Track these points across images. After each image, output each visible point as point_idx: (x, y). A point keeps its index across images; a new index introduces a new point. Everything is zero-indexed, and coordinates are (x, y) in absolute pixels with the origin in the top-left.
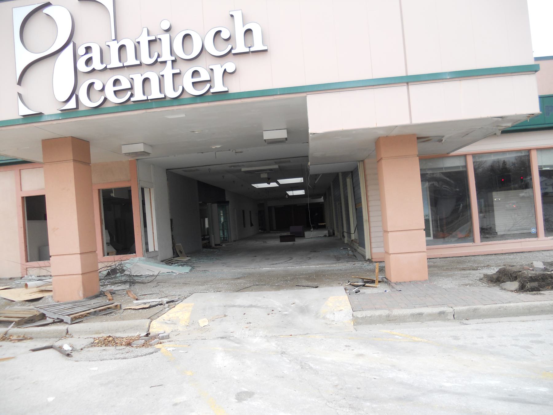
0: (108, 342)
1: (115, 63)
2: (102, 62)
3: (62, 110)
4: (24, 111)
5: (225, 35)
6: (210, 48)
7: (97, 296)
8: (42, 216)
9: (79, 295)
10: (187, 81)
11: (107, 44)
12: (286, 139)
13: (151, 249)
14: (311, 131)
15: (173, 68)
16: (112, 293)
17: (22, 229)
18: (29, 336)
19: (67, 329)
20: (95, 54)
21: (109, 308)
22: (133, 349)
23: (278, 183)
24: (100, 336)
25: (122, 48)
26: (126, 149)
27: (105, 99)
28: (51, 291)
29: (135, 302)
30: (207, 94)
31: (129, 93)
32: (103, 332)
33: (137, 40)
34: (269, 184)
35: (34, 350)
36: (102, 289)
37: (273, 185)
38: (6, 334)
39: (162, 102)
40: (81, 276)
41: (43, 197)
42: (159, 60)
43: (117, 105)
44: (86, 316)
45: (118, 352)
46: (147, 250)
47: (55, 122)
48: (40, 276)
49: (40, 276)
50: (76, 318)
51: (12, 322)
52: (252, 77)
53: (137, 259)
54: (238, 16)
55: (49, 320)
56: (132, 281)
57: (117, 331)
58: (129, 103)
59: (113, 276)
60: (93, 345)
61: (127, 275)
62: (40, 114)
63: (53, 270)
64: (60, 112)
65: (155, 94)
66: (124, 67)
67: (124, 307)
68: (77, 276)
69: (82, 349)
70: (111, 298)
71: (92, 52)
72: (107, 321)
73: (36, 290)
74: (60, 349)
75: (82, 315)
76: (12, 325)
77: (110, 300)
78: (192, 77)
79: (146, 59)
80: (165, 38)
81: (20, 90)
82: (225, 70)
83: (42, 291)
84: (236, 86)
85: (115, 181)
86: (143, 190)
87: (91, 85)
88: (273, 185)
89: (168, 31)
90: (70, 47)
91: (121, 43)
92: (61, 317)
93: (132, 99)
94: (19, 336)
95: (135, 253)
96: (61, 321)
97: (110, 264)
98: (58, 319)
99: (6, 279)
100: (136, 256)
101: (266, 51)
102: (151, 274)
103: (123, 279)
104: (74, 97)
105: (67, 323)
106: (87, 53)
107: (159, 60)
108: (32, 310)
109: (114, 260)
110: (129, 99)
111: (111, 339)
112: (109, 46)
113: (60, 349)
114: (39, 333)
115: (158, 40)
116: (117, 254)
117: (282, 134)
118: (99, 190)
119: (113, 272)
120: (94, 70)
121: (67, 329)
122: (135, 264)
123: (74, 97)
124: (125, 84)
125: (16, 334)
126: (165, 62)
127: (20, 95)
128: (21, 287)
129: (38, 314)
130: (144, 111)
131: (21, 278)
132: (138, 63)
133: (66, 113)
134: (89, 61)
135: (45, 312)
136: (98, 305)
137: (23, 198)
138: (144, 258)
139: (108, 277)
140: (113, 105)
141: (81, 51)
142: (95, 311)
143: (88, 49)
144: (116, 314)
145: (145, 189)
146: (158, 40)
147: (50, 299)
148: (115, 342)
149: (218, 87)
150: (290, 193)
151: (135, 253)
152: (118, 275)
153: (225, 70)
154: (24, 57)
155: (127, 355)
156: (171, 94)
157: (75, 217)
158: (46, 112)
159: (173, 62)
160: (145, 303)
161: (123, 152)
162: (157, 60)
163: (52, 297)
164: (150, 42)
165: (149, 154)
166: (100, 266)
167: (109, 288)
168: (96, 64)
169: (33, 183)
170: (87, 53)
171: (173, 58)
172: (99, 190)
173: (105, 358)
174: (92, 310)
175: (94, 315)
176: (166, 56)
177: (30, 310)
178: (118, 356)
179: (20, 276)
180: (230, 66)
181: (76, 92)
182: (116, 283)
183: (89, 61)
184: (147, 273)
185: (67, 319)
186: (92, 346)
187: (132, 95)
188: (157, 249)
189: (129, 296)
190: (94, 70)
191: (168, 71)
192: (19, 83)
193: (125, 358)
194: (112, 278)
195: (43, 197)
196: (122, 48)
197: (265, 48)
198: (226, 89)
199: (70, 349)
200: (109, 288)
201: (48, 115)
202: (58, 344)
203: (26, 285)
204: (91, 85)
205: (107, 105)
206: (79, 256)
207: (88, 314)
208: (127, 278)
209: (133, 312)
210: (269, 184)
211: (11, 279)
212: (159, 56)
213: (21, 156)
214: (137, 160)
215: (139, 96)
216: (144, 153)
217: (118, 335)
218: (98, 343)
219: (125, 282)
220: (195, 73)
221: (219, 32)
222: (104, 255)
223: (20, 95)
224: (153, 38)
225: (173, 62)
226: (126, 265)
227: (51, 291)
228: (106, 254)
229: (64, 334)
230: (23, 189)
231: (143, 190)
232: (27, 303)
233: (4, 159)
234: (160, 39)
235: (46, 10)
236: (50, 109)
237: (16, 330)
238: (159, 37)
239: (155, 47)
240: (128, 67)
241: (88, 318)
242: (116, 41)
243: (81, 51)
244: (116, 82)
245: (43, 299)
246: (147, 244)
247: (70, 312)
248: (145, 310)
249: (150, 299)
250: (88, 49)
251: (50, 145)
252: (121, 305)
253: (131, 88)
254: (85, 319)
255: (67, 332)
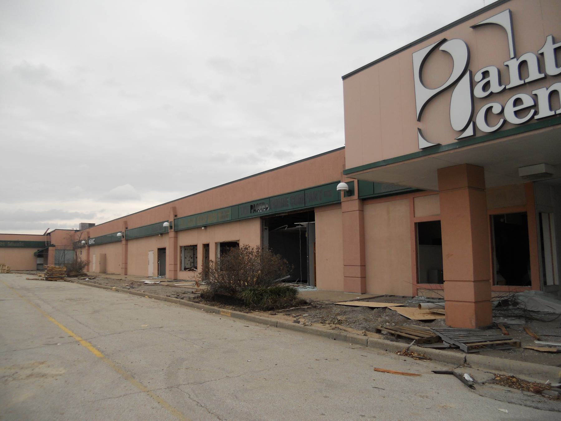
0: (511, 382)
1: (515, 81)
2: (500, 84)
4: (424, 144)
7: (489, 328)
8: (438, 242)
9: (471, 323)
10: (509, 111)
11: (506, 64)
13: (550, 282)
16: (507, 326)
18: (428, 357)
19: (465, 358)
20: (493, 78)
21: (506, 344)
22: (543, 399)
24: (501, 373)
25: (523, 65)
26: (523, 172)
27: (505, 122)
28: (444, 315)
29: (537, 342)
31: (532, 111)
32: (504, 370)
33: (540, 52)
35: (436, 372)
36: (495, 320)
38: (408, 349)
40: (473, 304)
43: (517, 126)
44: (482, 347)
45: (526, 398)
46: (545, 283)
47: (452, 152)
48: (429, 298)
49: (429, 298)
50: (472, 348)
51: (413, 340)
53: (533, 292)
55: (446, 345)
56: (529, 316)
57: (521, 372)
59: (505, 308)
60: (494, 381)
61: (521, 309)
62: (438, 146)
63: (446, 295)
64: (456, 141)
66: (525, 84)
67: (524, 345)
68: (469, 304)
69: (483, 383)
70: (506, 332)
71: (489, 76)
72: (506, 358)
73: (428, 311)
74: (460, 377)
75: (478, 346)
76: (413, 342)
77: (505, 334)
83: (434, 313)
85: (506, 206)
86: (540, 214)
90: (467, 76)
91: (521, 59)
92: (457, 344)
93: (536, 117)
94: (419, 354)
95: (531, 285)
96: (457, 348)
97: (502, 294)
98: (454, 345)
99: (400, 297)
100: (531, 289)
102: (551, 311)
103: (517, 312)
104: (471, 124)
105: (463, 351)
106: (484, 78)
108: (426, 331)
109: (501, 292)
110: (533, 117)
111: (514, 380)
113: (460, 377)
114: (438, 355)
116: (507, 284)
118: (490, 216)
119: (504, 304)
120: (492, 93)
121: (465, 358)
122: (531, 298)
123: (471, 124)
124: (528, 101)
125: (416, 351)
127: (420, 130)
128: (414, 306)
129: (434, 336)
130: (551, 128)
131: (413, 298)
134: (486, 86)
135: (440, 335)
136: (494, 338)
137: (415, 223)
138: (542, 292)
139: (499, 308)
140: (514, 127)
141: (478, 76)
142: (492, 345)
143: (486, 74)
144: (515, 351)
145: (543, 214)
147: (442, 323)
148: (520, 385)
151: (531, 285)
152: (511, 307)
154: (423, 94)
155: (540, 405)
157: (470, 244)
158: (444, 143)
160: (550, 346)
161: (521, 175)
163: (444, 321)
165: (551, 175)
166: (493, 295)
167: (502, 320)
168: (495, 87)
169: (427, 209)
170: (484, 78)
172: (490, 216)
173: (513, 401)
174: (489, 343)
175: (491, 348)
177: (427, 330)
178: (528, 403)
179: (412, 296)
181: (473, 119)
182: (509, 317)
183: (486, 86)
184: (546, 310)
185: (464, 347)
186: (494, 383)
187: (536, 113)
188: (557, 283)
189: (527, 333)
190: (492, 93)
192: (419, 119)
193: (538, 408)
194: (504, 310)
196: (523, 65)
199: (471, 380)
200: (502, 320)
201: (445, 146)
202: (458, 371)
203: (420, 306)
204: (490, 109)
205: (507, 128)
206: (472, 284)
207: (484, 345)
208: (521, 313)
209: (537, 354)
211: (403, 297)
213: (416, 186)
214: (534, 182)
216: (546, 175)
217: (522, 377)
218: (500, 381)
219: (519, 317)
220: (518, 102)
222: (494, 285)
223: (420, 130)
226: (521, 298)
227: (444, 315)
228: (496, 283)
229: (462, 362)
230: (416, 215)
231: (540, 214)
232: (421, 323)
233: (400, 188)
235: (442, 48)
236: (447, 139)
237: (416, 348)
241: (485, 350)
242: (515, 59)
243: (478, 76)
245: (436, 322)
246: (545, 275)
247: (465, 340)
249: (555, 341)
252: (520, 343)
254: (481, 350)
255: (465, 361)
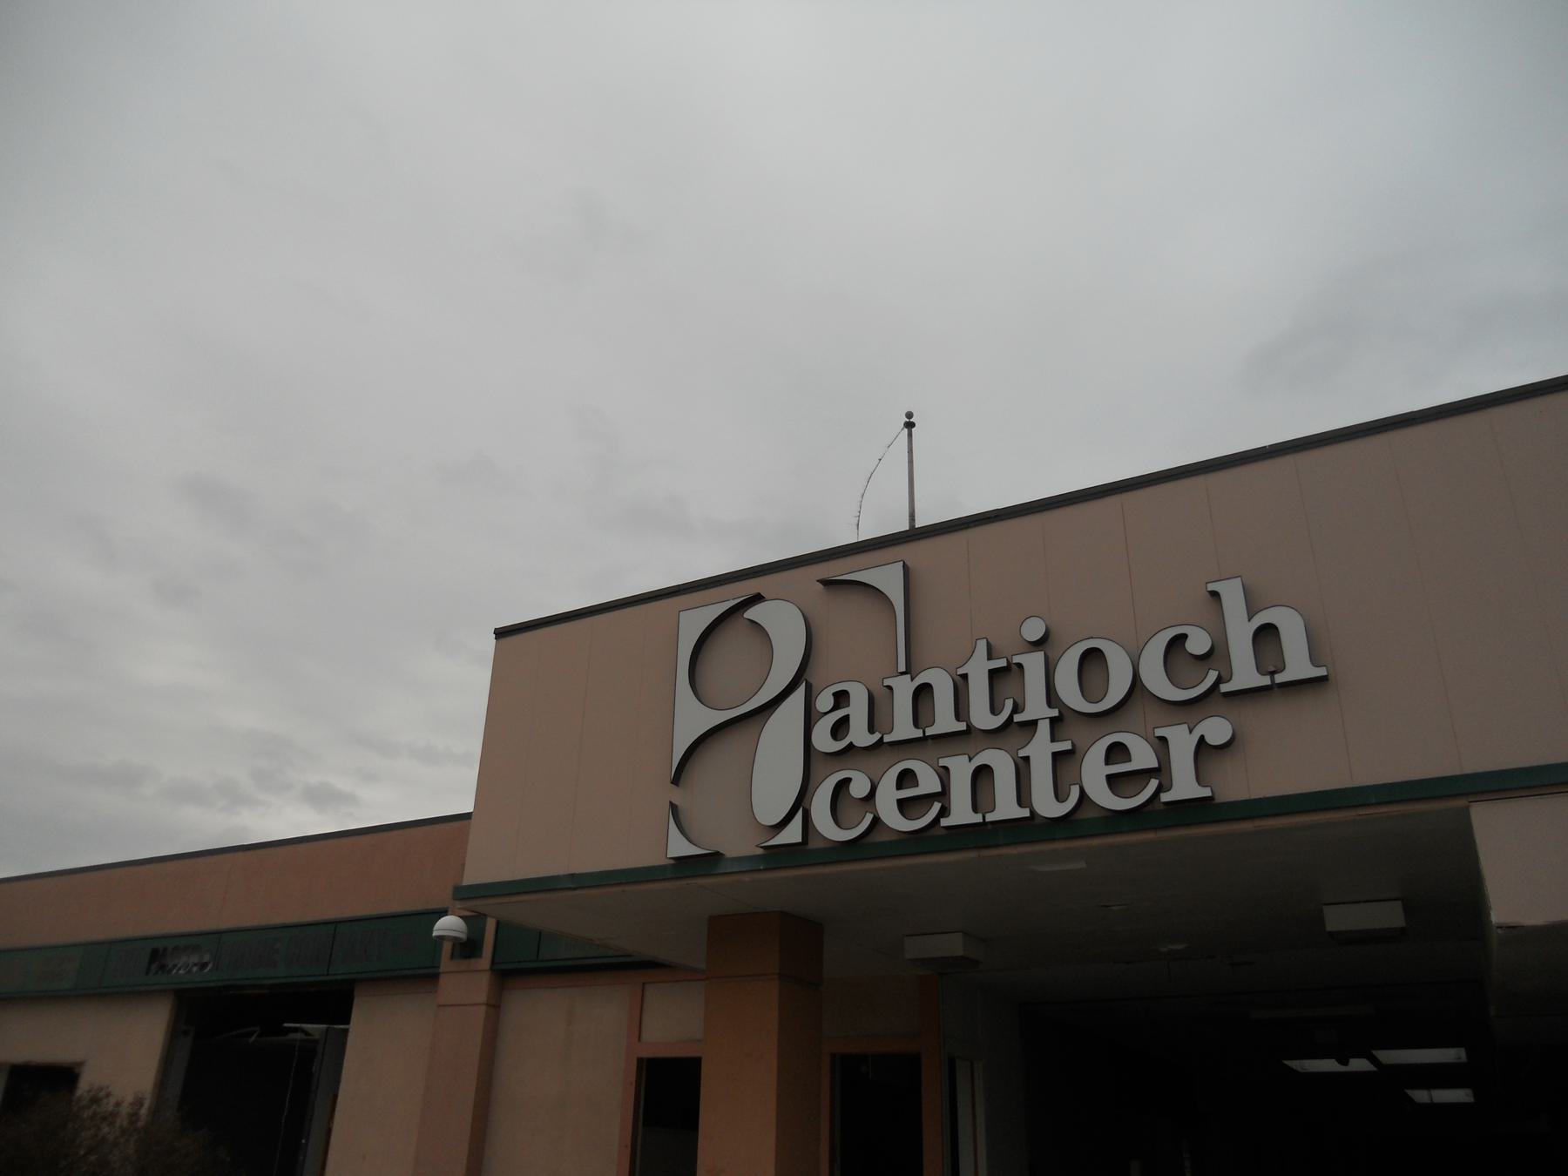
1: (904, 728)
2: (871, 730)
3: (765, 848)
4: (680, 847)
5: (1198, 643)
6: (1157, 682)
8: (689, 1121)
10: (1094, 772)
12: (1403, 931)
14: (1496, 917)
15: (1053, 740)
17: (629, 1150)
20: (857, 711)
23: (1374, 1060)
25: (923, 693)
27: (876, 821)
30: (1149, 808)
31: (937, 806)
34: (1344, 1061)
37: (1359, 1065)
39: (1029, 828)
41: (696, 1062)
42: (1018, 718)
47: (746, 878)
52: (1290, 759)
54: (1232, 595)
58: (935, 832)
62: (716, 856)
64: (760, 851)
65: (1006, 808)
66: (925, 738)
78: (1108, 762)
79: (982, 718)
80: (1034, 664)
81: (677, 795)
82: (1202, 738)
84: (1236, 785)
87: (843, 784)
88: (1359, 1065)
89: (1038, 644)
91: (919, 680)
101: (1322, 680)
107: (1018, 718)
110: (936, 821)
112: (890, 688)
115: (1015, 668)
117: (1390, 916)
120: (851, 746)
124: (928, 783)
126: (1033, 724)
127: (674, 808)
130: (972, 854)
132: (962, 726)
133: (778, 856)
140: (894, 837)
141: (824, 701)
143: (841, 698)
146: (1015, 668)
149: (1185, 786)
150: (1420, 1096)
153: (1202, 738)
154: (693, 719)
156: (1048, 806)
158: (730, 852)
159: (1053, 721)
162: (1011, 718)
164: (993, 674)
168: (859, 735)
169: (673, 1021)
171: (1055, 713)
176: (1036, 707)
180: (1217, 730)
187: (944, 812)
190: (851, 746)
191: (1041, 749)
192: (676, 780)
195: (696, 1062)
196: (923, 693)
197: (1322, 672)
198: (1206, 792)
201: (739, 859)
204: (843, 784)
205: (878, 837)
210: (1345, 1063)
212: (1017, 709)
215: (962, 813)
220: (1117, 752)
221: (1178, 641)
223: (674, 808)
224: (1002, 663)
225: (1053, 721)
230: (645, 1036)
234: (1020, 666)
235: (752, 613)
236: (738, 845)
238: (1016, 659)
239: (1007, 686)
240: (936, 737)
243: (824, 701)
244: (906, 779)
248: (248, 853)
250: (841, 698)
251: (728, 930)
253: (943, 795)
